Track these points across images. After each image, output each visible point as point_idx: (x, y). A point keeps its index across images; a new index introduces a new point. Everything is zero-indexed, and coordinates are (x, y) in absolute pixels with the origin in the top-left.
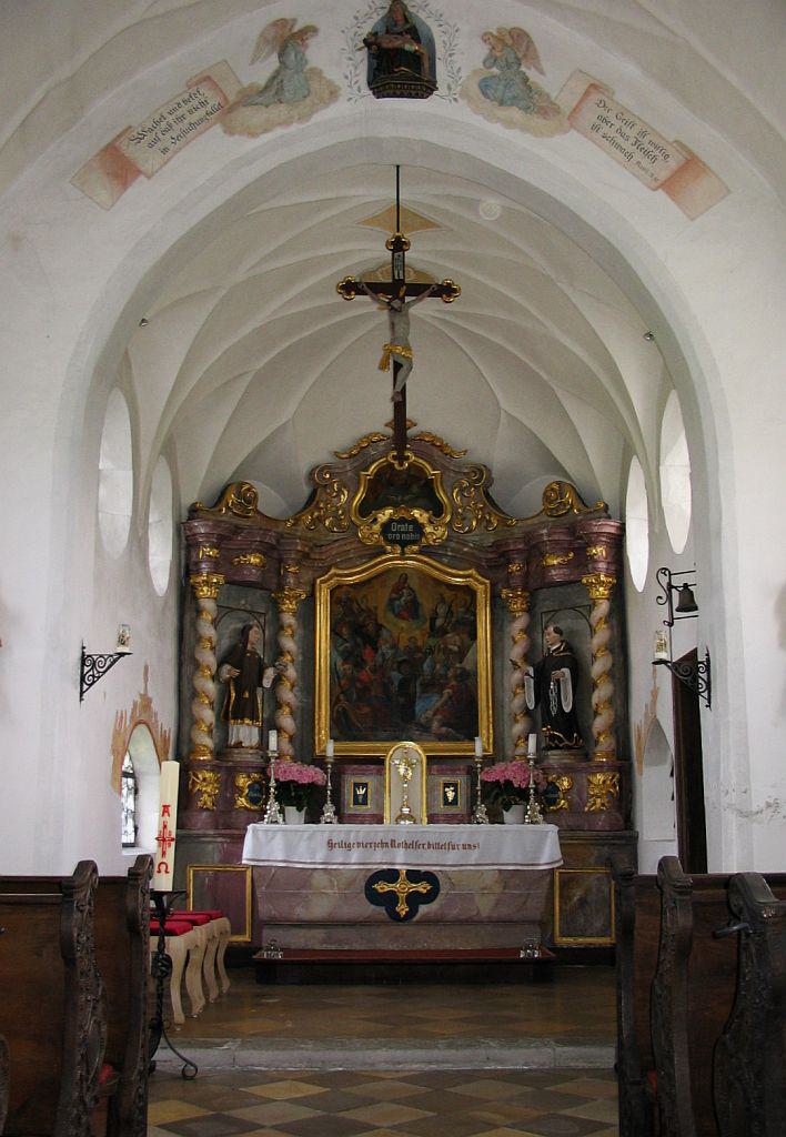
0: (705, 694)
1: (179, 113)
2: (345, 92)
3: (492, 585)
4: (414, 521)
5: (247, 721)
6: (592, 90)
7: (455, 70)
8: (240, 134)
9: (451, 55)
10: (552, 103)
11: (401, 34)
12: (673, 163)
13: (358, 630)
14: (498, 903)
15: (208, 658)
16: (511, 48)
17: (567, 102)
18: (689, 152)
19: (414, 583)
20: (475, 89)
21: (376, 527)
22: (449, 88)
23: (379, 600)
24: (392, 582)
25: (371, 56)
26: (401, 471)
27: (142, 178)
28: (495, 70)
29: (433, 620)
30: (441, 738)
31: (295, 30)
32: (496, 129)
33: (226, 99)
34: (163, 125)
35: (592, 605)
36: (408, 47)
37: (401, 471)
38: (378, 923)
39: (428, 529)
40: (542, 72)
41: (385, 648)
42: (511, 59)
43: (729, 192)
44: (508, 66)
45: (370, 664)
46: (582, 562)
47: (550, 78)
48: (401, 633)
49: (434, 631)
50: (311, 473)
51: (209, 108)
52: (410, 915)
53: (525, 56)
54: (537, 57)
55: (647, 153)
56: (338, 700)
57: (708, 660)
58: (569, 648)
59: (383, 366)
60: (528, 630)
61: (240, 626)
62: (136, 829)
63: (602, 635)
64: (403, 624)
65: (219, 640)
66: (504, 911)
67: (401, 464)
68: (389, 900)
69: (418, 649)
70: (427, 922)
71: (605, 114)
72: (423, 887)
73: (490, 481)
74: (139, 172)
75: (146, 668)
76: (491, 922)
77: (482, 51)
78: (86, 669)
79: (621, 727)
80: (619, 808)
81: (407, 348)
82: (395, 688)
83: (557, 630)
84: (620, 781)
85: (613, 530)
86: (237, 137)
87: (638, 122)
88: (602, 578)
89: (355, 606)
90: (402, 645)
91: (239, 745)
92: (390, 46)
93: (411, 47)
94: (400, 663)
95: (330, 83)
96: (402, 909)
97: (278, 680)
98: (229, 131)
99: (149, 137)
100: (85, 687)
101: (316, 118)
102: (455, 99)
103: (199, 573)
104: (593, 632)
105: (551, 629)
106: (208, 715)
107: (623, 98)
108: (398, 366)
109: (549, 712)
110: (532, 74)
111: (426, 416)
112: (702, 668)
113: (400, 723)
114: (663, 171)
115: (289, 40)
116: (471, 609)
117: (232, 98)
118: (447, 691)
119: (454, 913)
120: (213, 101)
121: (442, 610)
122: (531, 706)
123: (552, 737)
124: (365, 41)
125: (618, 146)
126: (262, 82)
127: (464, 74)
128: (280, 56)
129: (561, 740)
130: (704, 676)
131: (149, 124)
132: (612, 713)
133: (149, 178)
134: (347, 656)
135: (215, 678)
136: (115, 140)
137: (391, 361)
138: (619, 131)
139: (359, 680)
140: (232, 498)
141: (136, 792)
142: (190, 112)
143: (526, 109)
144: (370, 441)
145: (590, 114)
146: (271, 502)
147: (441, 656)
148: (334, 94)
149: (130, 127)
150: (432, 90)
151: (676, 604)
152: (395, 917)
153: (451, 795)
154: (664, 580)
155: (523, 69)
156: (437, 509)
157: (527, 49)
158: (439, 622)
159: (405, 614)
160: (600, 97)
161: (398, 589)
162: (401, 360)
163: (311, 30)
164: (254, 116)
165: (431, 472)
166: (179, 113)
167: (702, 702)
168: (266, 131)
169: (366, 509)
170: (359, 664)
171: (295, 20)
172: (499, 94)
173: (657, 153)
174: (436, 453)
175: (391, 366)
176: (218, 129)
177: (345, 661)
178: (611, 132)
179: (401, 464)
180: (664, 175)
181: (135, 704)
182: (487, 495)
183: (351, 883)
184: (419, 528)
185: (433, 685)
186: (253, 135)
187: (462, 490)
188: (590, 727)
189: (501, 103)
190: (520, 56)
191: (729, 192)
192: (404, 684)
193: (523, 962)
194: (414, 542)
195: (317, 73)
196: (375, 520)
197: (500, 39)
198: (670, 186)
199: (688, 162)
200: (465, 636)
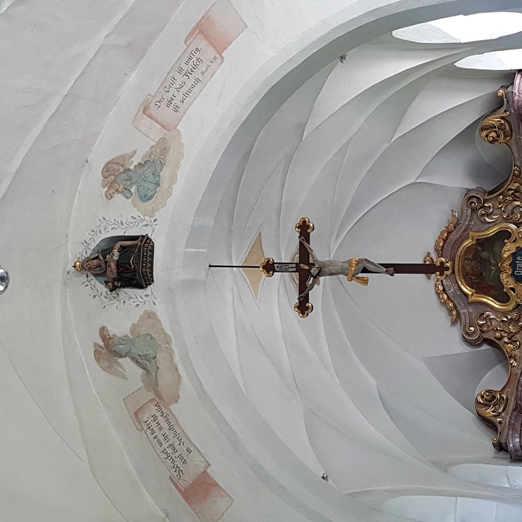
1: (161, 438)
2: (149, 307)
4: (514, 255)
6: (147, 113)
7: (133, 221)
8: (178, 390)
9: (122, 224)
10: (158, 142)
11: (106, 262)
12: (203, 44)
17: (156, 133)
22: (147, 225)
27: (209, 470)
28: (133, 190)
31: (102, 344)
33: (152, 400)
34: (170, 451)
36: (116, 258)
42: (125, 176)
47: (139, 145)
53: (122, 166)
54: (123, 156)
55: (195, 66)
59: (365, 281)
67: (447, 269)
71: (166, 101)
77: (119, 198)
81: (350, 262)
86: (180, 393)
92: (115, 271)
98: (176, 399)
99: (179, 463)
101: (168, 331)
102: (155, 221)
108: (365, 270)
110: (136, 160)
111: (420, 245)
115: (109, 350)
117: (152, 395)
120: (153, 410)
125: (190, 91)
127: (136, 213)
128: (121, 356)
133: (209, 465)
137: (360, 275)
138: (178, 89)
140: (489, 412)
143: (162, 165)
145: (165, 114)
146: (494, 379)
150: (148, 238)
155: (132, 167)
160: (152, 105)
162: (361, 267)
164: (165, 378)
166: (161, 438)
168: (177, 369)
169: (503, 298)
171: (95, 344)
172: (152, 186)
173: (194, 59)
174: (454, 236)
176: (173, 407)
179: (447, 269)
180: (212, 52)
182: (491, 193)
186: (179, 378)
189: (158, 184)
190: (122, 170)
195: (134, 328)
196: (513, 289)
198: (220, 47)
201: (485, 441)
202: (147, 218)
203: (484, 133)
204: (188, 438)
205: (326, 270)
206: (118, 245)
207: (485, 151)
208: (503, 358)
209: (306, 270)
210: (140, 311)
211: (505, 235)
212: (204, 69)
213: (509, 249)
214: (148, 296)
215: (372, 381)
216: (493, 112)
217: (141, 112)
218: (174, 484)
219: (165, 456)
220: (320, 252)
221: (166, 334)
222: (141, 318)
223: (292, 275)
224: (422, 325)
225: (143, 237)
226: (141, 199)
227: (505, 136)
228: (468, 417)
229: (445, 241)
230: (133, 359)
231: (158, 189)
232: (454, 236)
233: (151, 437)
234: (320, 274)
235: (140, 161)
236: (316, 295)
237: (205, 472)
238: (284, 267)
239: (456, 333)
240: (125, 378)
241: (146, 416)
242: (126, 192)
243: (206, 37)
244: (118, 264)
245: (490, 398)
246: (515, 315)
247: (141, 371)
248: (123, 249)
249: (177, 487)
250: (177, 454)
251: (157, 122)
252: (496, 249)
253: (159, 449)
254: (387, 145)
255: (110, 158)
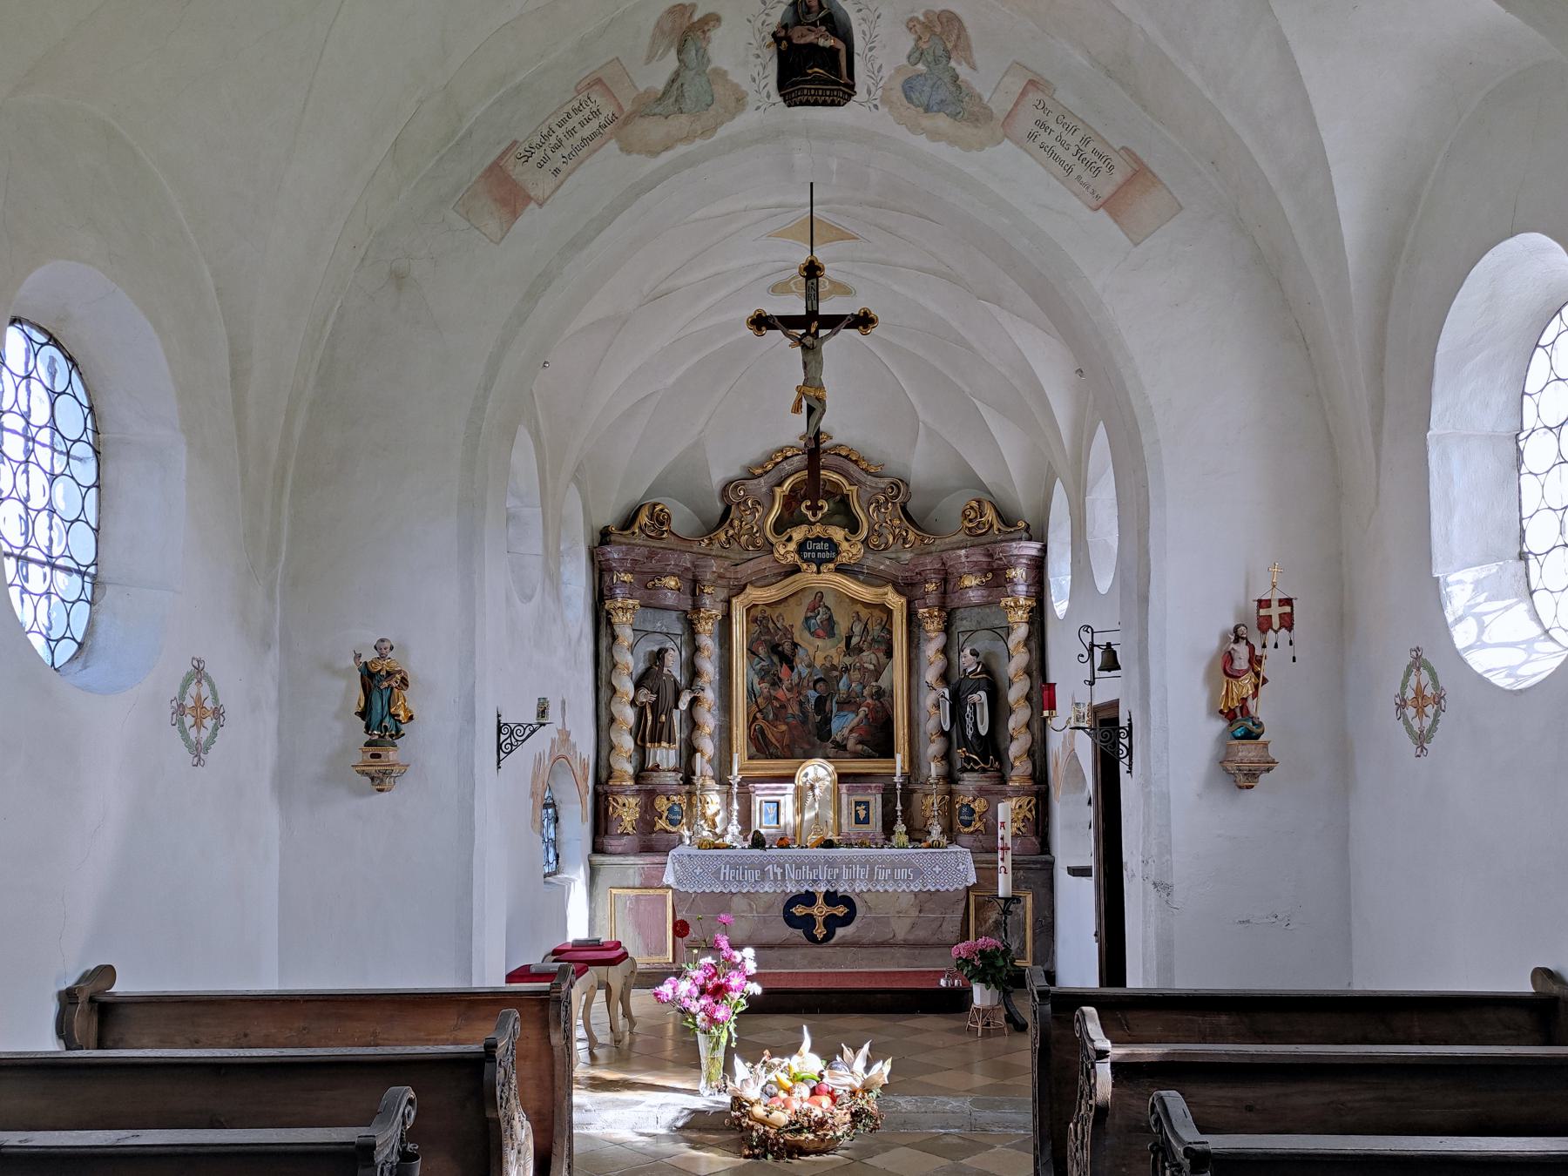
0: (1126, 760)
1: (569, 125)
2: (752, 98)
3: (909, 603)
4: (830, 540)
5: (664, 744)
6: (1030, 87)
7: (876, 67)
8: (639, 152)
9: (871, 49)
10: (986, 108)
11: (814, 24)
12: (1118, 177)
13: (775, 649)
14: (913, 926)
15: (626, 686)
16: (940, 36)
17: (1000, 104)
18: (1137, 160)
19: (829, 601)
20: (898, 95)
21: (792, 546)
22: (869, 92)
23: (794, 617)
24: (808, 600)
25: (781, 54)
26: (815, 484)
27: (532, 205)
28: (921, 67)
29: (849, 639)
30: (857, 755)
31: (696, 18)
32: (921, 142)
33: (620, 107)
34: (553, 140)
35: (1009, 630)
36: (821, 42)
37: (815, 484)
38: (796, 946)
39: (845, 546)
40: (974, 68)
41: (801, 667)
42: (940, 52)
43: (1181, 208)
44: (936, 61)
45: (786, 683)
46: (996, 577)
47: (985, 76)
48: (817, 652)
49: (849, 649)
50: (724, 489)
51: (602, 119)
52: (827, 938)
53: (955, 46)
54: (969, 47)
55: (1089, 165)
56: (755, 718)
57: (1130, 725)
58: (987, 669)
59: (797, 409)
60: (945, 651)
61: (656, 649)
62: (557, 856)
63: (1020, 659)
64: (819, 642)
65: (636, 664)
66: (921, 934)
67: (814, 515)
68: (807, 923)
69: (834, 667)
70: (844, 944)
71: (1044, 118)
72: (841, 911)
73: (909, 495)
74: (529, 199)
75: (563, 702)
76: (907, 944)
77: (907, 43)
78: (503, 737)
79: (1038, 753)
80: (1036, 834)
81: (821, 387)
82: (810, 707)
83: (974, 653)
84: (1036, 806)
85: (1034, 553)
86: (635, 156)
87: (1080, 126)
88: (1022, 602)
89: (771, 625)
90: (818, 664)
91: (656, 768)
92: (802, 41)
93: (828, 42)
94: (816, 682)
95: (736, 87)
96: (820, 931)
97: (695, 701)
98: (627, 149)
99: (538, 155)
100: (502, 755)
101: (722, 132)
102: (876, 107)
103: (613, 597)
104: (1010, 657)
105: (967, 651)
106: (627, 743)
107: (1066, 97)
108: (811, 410)
109: (965, 736)
110: (962, 70)
111: (839, 426)
112: (1123, 733)
113: (813, 737)
114: (1106, 185)
115: (689, 33)
116: (887, 627)
117: (628, 108)
118: (863, 710)
119: (871, 935)
120: (607, 111)
121: (857, 629)
122: (947, 728)
123: (968, 760)
124: (774, 35)
125: (1056, 158)
126: (660, 86)
127: (887, 72)
128: (679, 52)
129: (976, 763)
130: (1126, 742)
131: (537, 140)
132: (1029, 737)
133: (541, 205)
134: (763, 674)
135: (633, 703)
136: (501, 157)
137: (804, 403)
138: (1059, 139)
139: (776, 699)
140: (644, 518)
141: (557, 820)
142: (582, 124)
143: (954, 116)
144: (783, 454)
145: (1026, 121)
146: (681, 518)
147: (856, 675)
148: (740, 101)
149: (515, 142)
150: (850, 96)
151: (1098, 663)
152: (812, 939)
153: (862, 814)
154: (1087, 638)
155: (953, 64)
156: (853, 526)
157: (958, 37)
158: (854, 641)
159: (820, 632)
160: (1040, 96)
161: (813, 608)
162: (815, 404)
163: (712, 20)
164: (654, 129)
165: (847, 487)
166: (569, 125)
167: (1123, 768)
168: (667, 149)
169: (780, 527)
170: (776, 682)
171: (694, 6)
172: (924, 99)
173: (1100, 164)
174: (852, 468)
175: (805, 409)
176: (613, 145)
177: (762, 679)
178: (1050, 141)
179: (814, 515)
180: (1106, 191)
181: (553, 741)
182: (904, 509)
183: (769, 907)
184: (834, 547)
185: (848, 703)
186: (654, 153)
187: (878, 508)
188: (1007, 749)
189: (927, 109)
190: (950, 46)
191: (1181, 208)
192: (820, 702)
193: (942, 990)
194: (830, 560)
195: (721, 74)
196: (790, 539)
197: (928, 27)
198: (1112, 205)
199: (1136, 173)
200: (881, 655)
201: (609, 515)
202: (879, 92)
203: (974, 504)
204: (574, 170)
205: (810, 357)
206: (841, 46)
207: (952, 507)
208: (710, 530)
209: (809, 327)
210: (746, 86)
211: (853, 526)
212: (1084, 180)
213: (838, 534)
214: (768, 96)
215: (671, 380)
216: (999, 514)
217: (1030, 76)
218: (508, 149)
219: (545, 132)
220: (837, 346)
221: (715, 129)
222: (736, 87)
223: (801, 206)
224: (743, 423)
225: (852, 87)
226: (908, 81)
227: (970, 529)
228: (636, 494)
229: (846, 457)
230: (677, 74)
231: (921, 110)
232: (852, 468)
233: (568, 108)
234: (805, 348)
235: (962, 77)
236: (776, 335)
237: (529, 199)
238: (812, 295)
239: (735, 472)
240: (649, 59)
241: (599, 99)
242: (917, 54)
243: (1129, 182)
244: (813, 47)
245: (660, 520)
246: (760, 542)
247: (661, 87)
248: (833, 52)
249: (504, 153)
250: (549, 153)
251: (1016, 104)
252: (837, 518)
253: (553, 122)
254: (967, 390)
255: (966, 24)
